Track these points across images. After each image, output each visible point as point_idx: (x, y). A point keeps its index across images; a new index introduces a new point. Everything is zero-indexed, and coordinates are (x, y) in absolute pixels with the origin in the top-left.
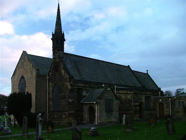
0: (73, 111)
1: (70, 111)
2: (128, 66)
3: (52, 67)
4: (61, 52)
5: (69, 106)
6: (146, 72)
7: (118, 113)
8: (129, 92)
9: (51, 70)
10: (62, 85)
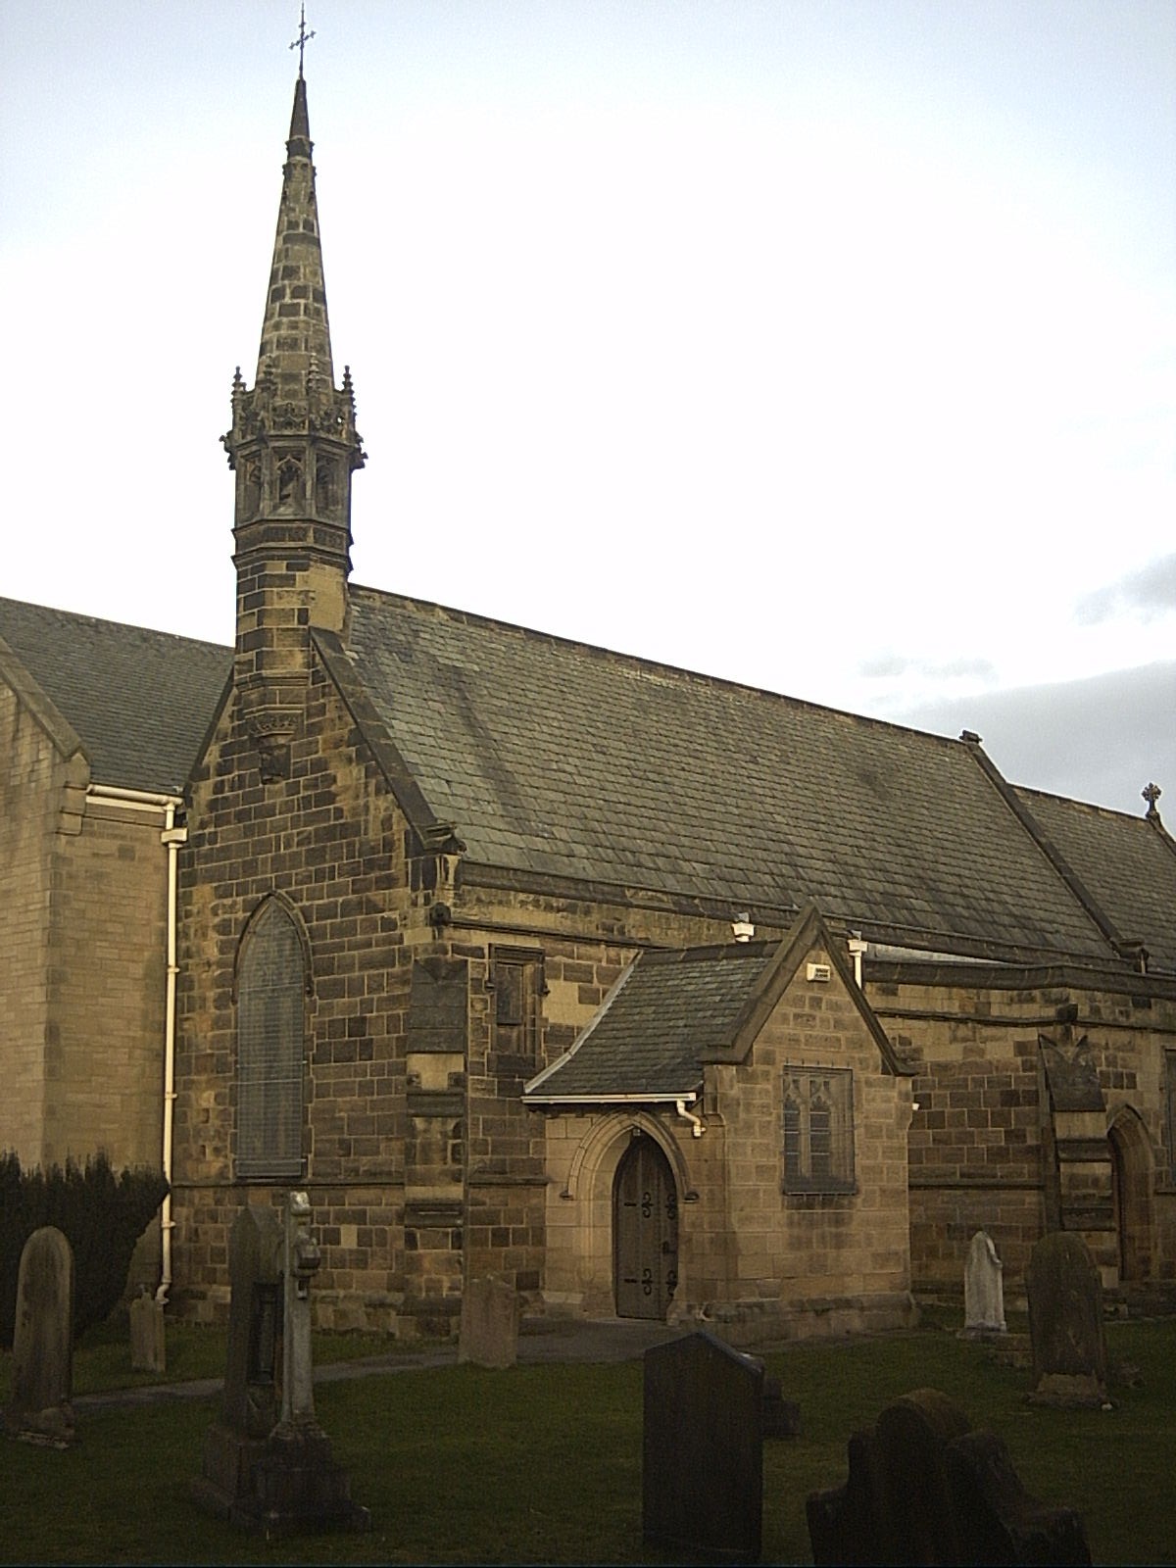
0: (456, 1178)
1: (425, 1180)
2: (966, 735)
3: (225, 723)
4: (320, 579)
5: (412, 1131)
6: (1141, 810)
7: (901, 1217)
8: (998, 1003)
9: (213, 757)
10: (327, 912)
